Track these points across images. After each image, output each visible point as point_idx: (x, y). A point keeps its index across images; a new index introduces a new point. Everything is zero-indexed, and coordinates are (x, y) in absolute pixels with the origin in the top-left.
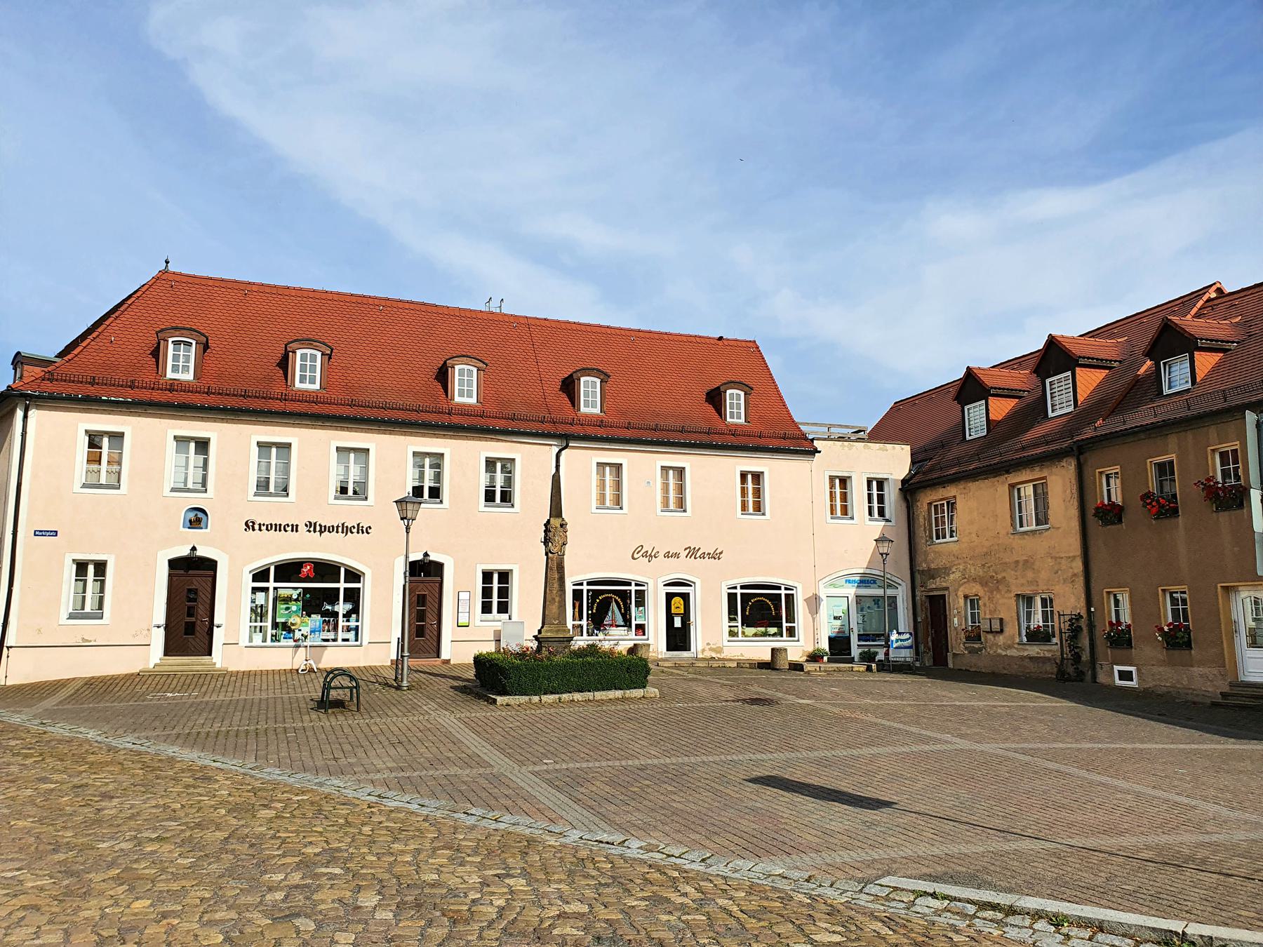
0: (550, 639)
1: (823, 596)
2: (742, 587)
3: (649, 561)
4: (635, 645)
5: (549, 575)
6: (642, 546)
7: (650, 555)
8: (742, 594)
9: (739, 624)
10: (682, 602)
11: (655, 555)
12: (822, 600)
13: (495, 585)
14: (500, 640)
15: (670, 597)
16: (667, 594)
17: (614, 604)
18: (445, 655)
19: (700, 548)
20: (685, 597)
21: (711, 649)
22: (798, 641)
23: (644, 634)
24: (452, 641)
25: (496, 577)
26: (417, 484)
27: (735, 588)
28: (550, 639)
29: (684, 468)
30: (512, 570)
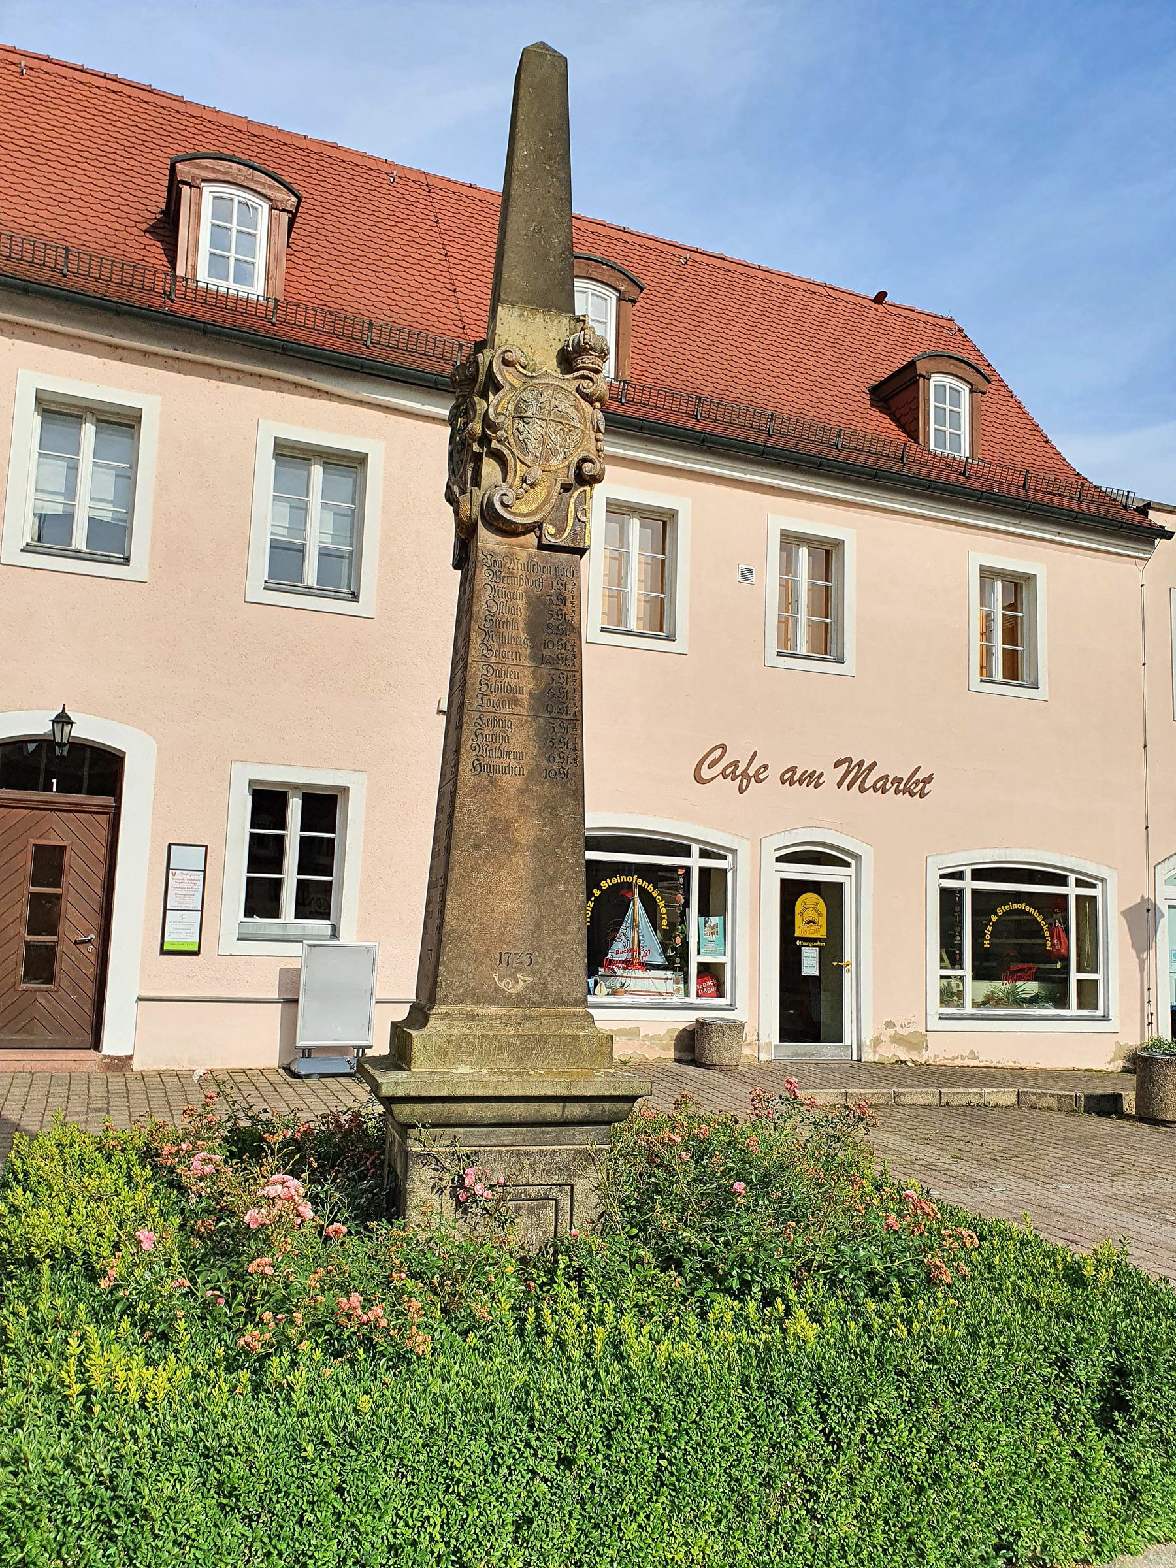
0: (470, 1111)
1: (1163, 906)
2: (978, 875)
3: (741, 791)
4: (701, 1025)
5: (476, 671)
6: (724, 747)
7: (745, 775)
8: (975, 893)
9: (967, 972)
10: (822, 907)
11: (757, 772)
12: (1163, 916)
13: (293, 833)
14: (296, 1001)
15: (791, 891)
16: (785, 883)
17: (637, 909)
18: (112, 1044)
19: (874, 764)
20: (832, 894)
21: (897, 1040)
22: (1105, 1018)
23: (720, 993)
24: (140, 999)
25: (295, 807)
26: (55, 508)
27: (958, 876)
28: (470, 1111)
29: (838, 544)
30: (345, 790)
